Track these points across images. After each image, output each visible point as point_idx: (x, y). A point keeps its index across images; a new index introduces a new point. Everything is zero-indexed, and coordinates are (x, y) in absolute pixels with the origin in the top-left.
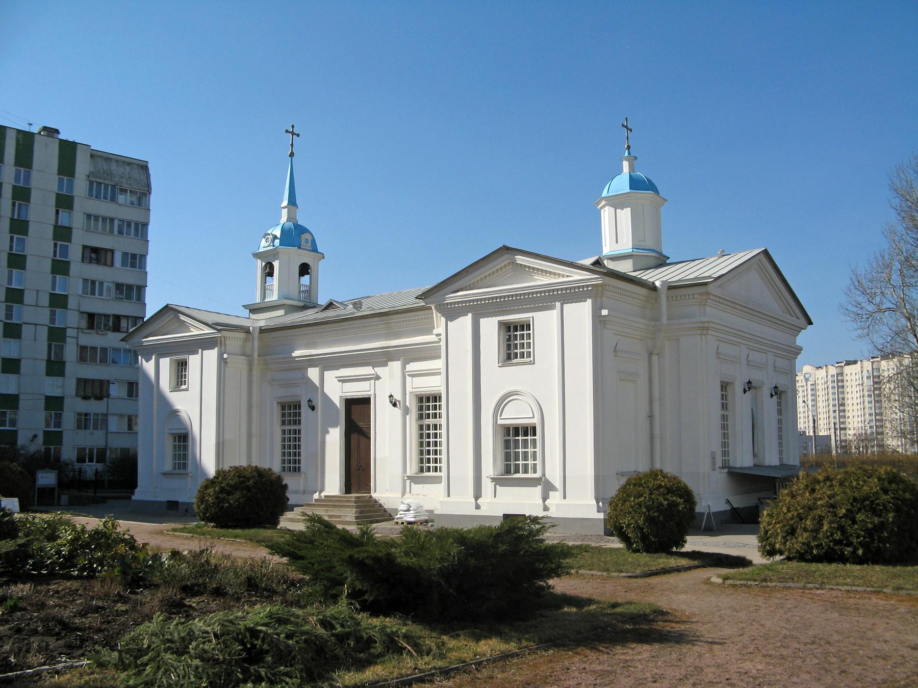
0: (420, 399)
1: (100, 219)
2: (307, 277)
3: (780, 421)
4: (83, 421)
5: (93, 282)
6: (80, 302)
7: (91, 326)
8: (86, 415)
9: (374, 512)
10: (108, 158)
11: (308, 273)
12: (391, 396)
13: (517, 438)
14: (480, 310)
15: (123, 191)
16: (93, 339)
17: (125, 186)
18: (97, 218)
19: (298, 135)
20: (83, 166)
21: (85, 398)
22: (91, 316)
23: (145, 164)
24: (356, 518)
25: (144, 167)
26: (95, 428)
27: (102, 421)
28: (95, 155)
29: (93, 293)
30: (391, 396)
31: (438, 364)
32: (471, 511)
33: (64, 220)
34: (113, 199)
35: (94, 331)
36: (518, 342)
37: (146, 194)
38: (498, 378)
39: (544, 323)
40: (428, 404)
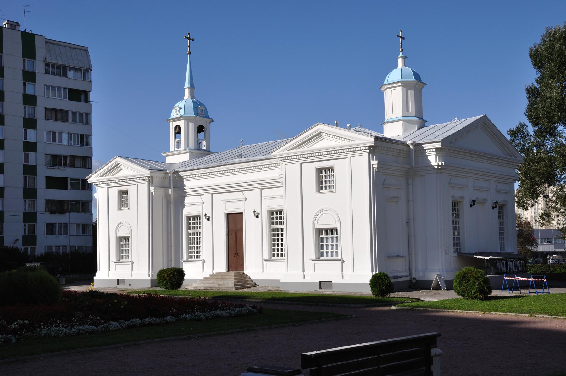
0: (272, 213)
1: (56, 88)
2: (202, 134)
3: (501, 224)
4: (51, 229)
5: (54, 133)
6: (46, 148)
7: (54, 164)
8: (53, 224)
9: (244, 281)
10: (58, 44)
11: (203, 131)
12: (255, 211)
13: (326, 236)
14: (304, 159)
15: (71, 69)
16: (57, 172)
17: (72, 65)
18: (54, 88)
19: (193, 40)
20: (40, 52)
21: (52, 212)
22: (54, 157)
23: (85, 48)
24: (235, 285)
25: (85, 50)
26: (60, 233)
27: (64, 229)
28: (48, 42)
29: (54, 140)
30: (255, 211)
31: (280, 191)
32: (301, 280)
33: (30, 90)
34: (65, 75)
35: (57, 167)
36: (324, 180)
37: (88, 71)
38: (315, 200)
39: (341, 167)
40: (276, 216)
